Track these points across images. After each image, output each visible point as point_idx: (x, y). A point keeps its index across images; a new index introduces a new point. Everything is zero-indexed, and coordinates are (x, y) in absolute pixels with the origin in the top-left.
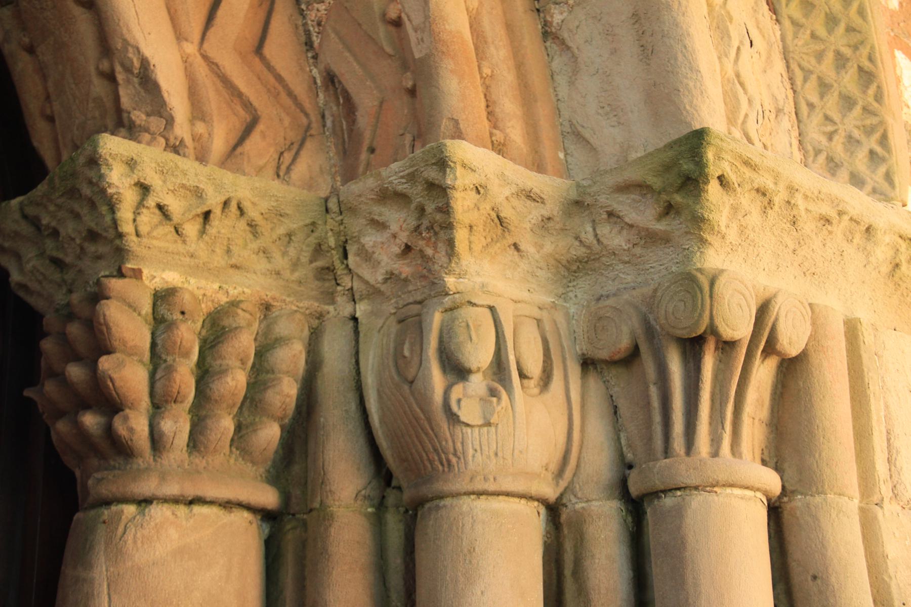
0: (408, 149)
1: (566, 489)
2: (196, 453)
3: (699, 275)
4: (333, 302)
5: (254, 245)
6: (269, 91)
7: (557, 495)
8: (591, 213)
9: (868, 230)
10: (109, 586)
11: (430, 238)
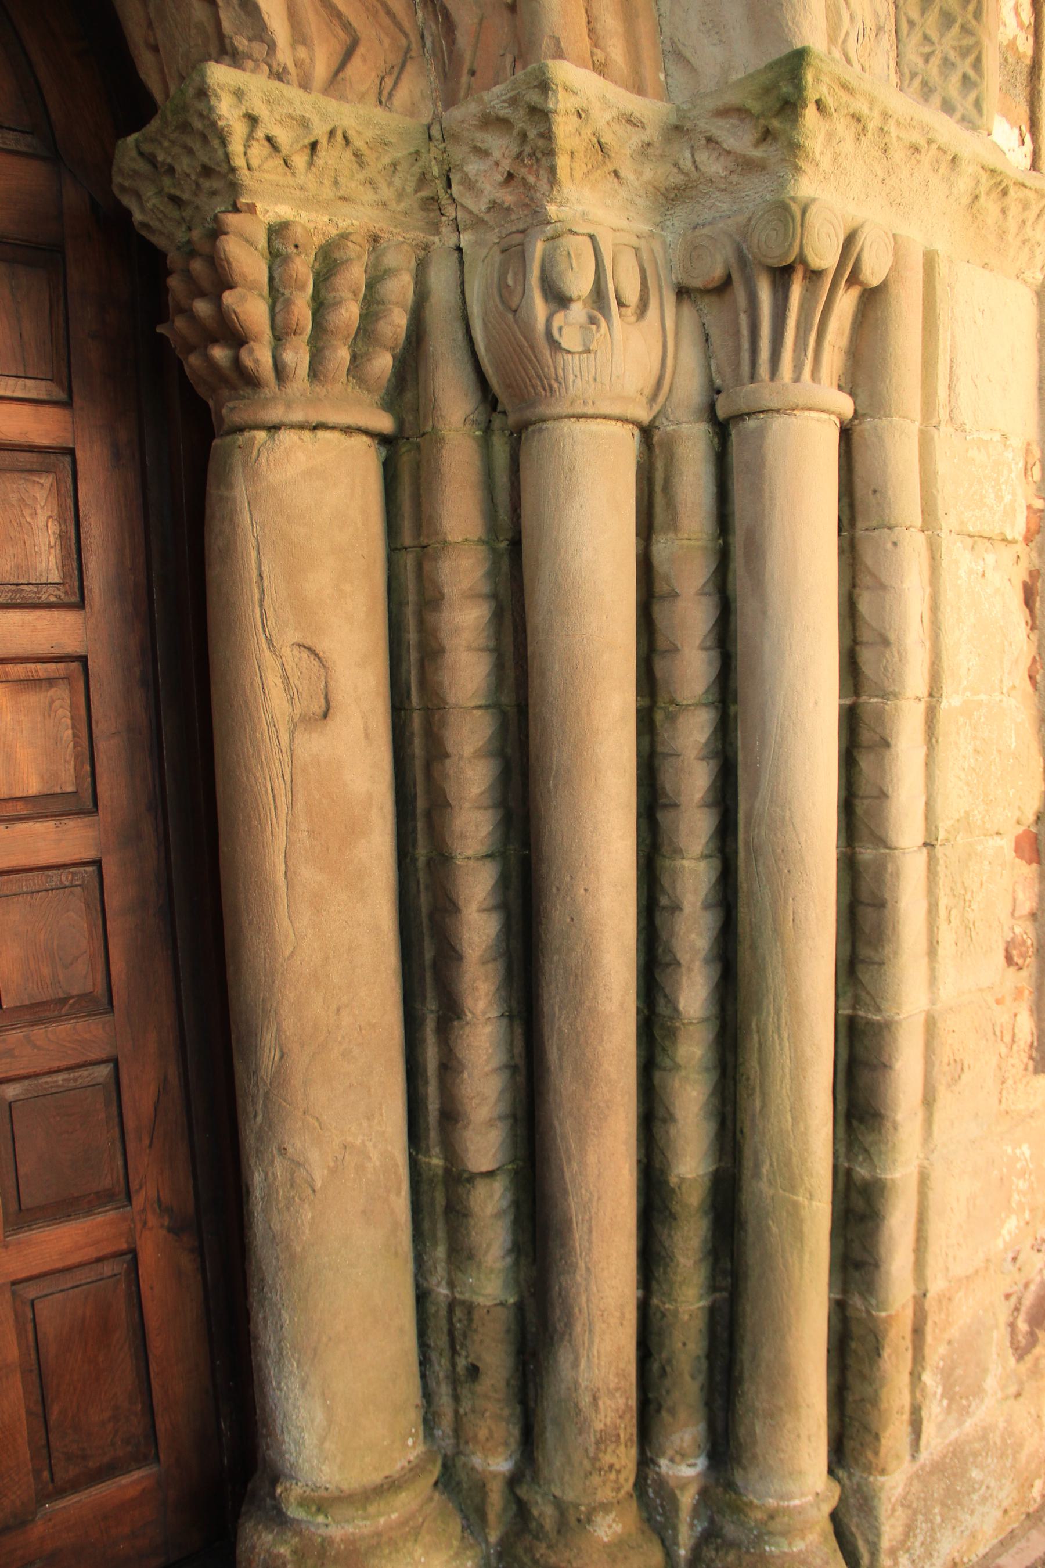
0: (509, 71)
1: (658, 413)
2: (316, 383)
3: (792, 204)
4: (438, 232)
5: (360, 176)
6: (367, 9)
7: (651, 418)
8: (690, 139)
9: (953, 159)
10: (249, 503)
11: (532, 165)
